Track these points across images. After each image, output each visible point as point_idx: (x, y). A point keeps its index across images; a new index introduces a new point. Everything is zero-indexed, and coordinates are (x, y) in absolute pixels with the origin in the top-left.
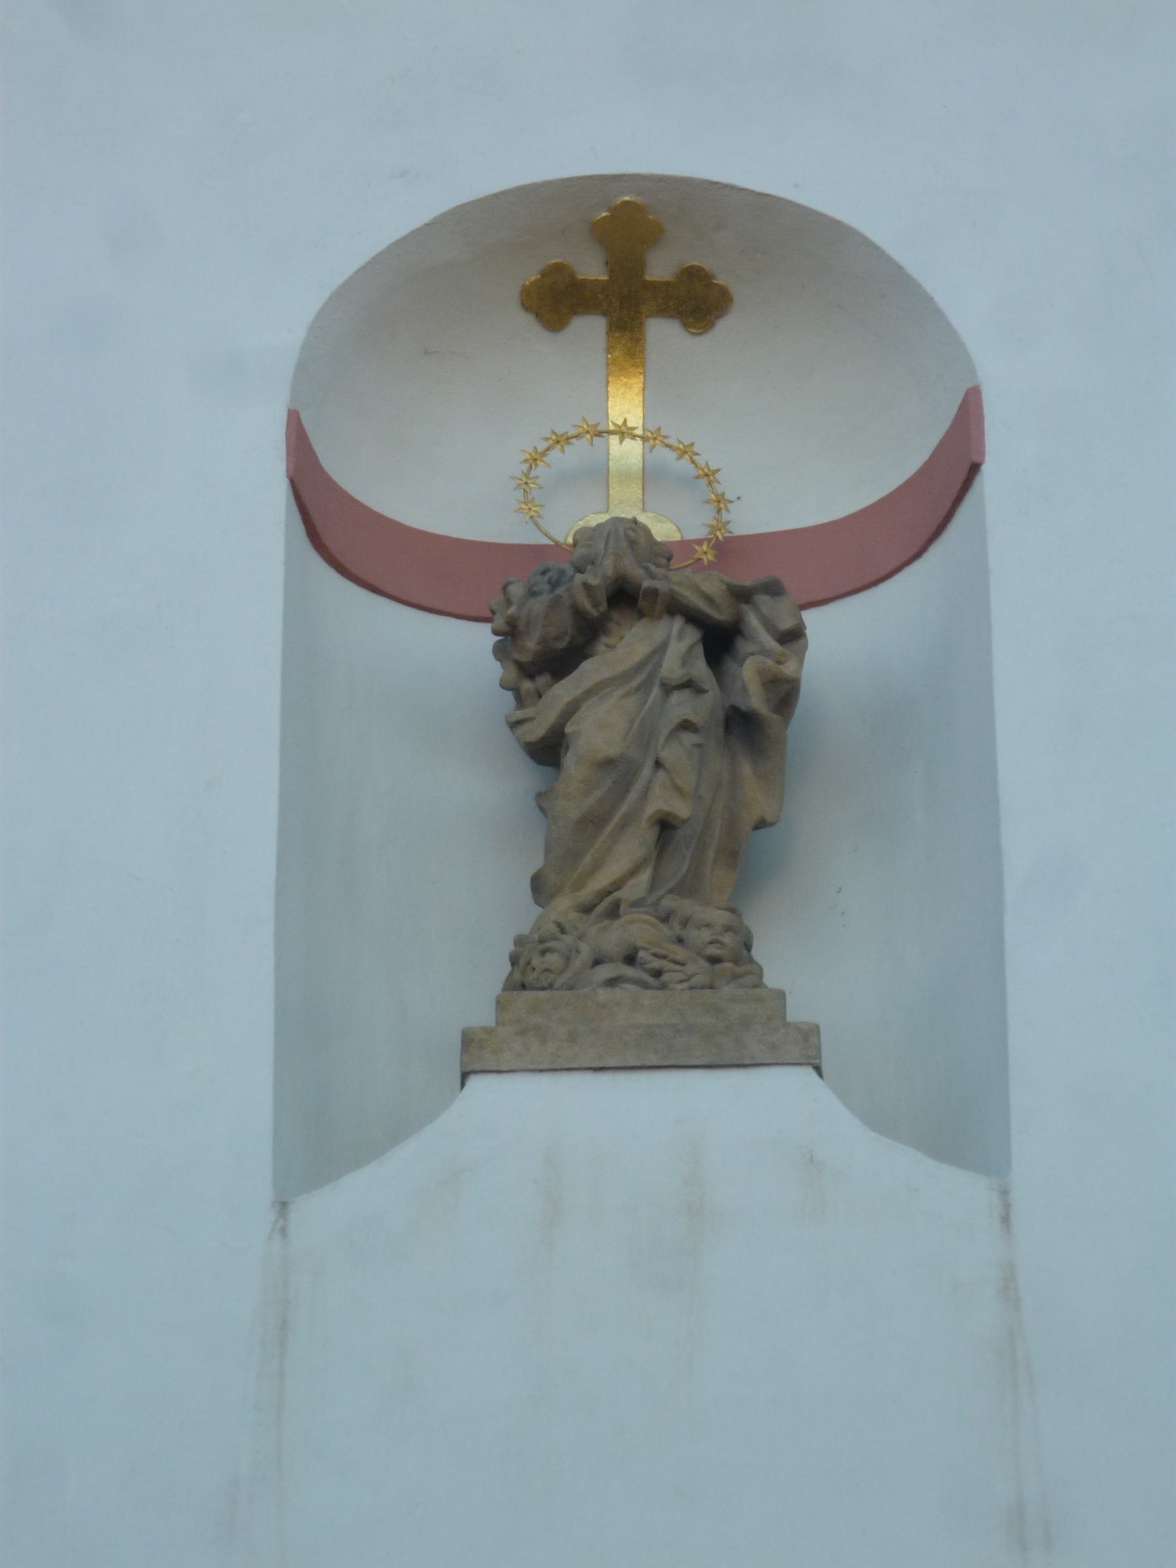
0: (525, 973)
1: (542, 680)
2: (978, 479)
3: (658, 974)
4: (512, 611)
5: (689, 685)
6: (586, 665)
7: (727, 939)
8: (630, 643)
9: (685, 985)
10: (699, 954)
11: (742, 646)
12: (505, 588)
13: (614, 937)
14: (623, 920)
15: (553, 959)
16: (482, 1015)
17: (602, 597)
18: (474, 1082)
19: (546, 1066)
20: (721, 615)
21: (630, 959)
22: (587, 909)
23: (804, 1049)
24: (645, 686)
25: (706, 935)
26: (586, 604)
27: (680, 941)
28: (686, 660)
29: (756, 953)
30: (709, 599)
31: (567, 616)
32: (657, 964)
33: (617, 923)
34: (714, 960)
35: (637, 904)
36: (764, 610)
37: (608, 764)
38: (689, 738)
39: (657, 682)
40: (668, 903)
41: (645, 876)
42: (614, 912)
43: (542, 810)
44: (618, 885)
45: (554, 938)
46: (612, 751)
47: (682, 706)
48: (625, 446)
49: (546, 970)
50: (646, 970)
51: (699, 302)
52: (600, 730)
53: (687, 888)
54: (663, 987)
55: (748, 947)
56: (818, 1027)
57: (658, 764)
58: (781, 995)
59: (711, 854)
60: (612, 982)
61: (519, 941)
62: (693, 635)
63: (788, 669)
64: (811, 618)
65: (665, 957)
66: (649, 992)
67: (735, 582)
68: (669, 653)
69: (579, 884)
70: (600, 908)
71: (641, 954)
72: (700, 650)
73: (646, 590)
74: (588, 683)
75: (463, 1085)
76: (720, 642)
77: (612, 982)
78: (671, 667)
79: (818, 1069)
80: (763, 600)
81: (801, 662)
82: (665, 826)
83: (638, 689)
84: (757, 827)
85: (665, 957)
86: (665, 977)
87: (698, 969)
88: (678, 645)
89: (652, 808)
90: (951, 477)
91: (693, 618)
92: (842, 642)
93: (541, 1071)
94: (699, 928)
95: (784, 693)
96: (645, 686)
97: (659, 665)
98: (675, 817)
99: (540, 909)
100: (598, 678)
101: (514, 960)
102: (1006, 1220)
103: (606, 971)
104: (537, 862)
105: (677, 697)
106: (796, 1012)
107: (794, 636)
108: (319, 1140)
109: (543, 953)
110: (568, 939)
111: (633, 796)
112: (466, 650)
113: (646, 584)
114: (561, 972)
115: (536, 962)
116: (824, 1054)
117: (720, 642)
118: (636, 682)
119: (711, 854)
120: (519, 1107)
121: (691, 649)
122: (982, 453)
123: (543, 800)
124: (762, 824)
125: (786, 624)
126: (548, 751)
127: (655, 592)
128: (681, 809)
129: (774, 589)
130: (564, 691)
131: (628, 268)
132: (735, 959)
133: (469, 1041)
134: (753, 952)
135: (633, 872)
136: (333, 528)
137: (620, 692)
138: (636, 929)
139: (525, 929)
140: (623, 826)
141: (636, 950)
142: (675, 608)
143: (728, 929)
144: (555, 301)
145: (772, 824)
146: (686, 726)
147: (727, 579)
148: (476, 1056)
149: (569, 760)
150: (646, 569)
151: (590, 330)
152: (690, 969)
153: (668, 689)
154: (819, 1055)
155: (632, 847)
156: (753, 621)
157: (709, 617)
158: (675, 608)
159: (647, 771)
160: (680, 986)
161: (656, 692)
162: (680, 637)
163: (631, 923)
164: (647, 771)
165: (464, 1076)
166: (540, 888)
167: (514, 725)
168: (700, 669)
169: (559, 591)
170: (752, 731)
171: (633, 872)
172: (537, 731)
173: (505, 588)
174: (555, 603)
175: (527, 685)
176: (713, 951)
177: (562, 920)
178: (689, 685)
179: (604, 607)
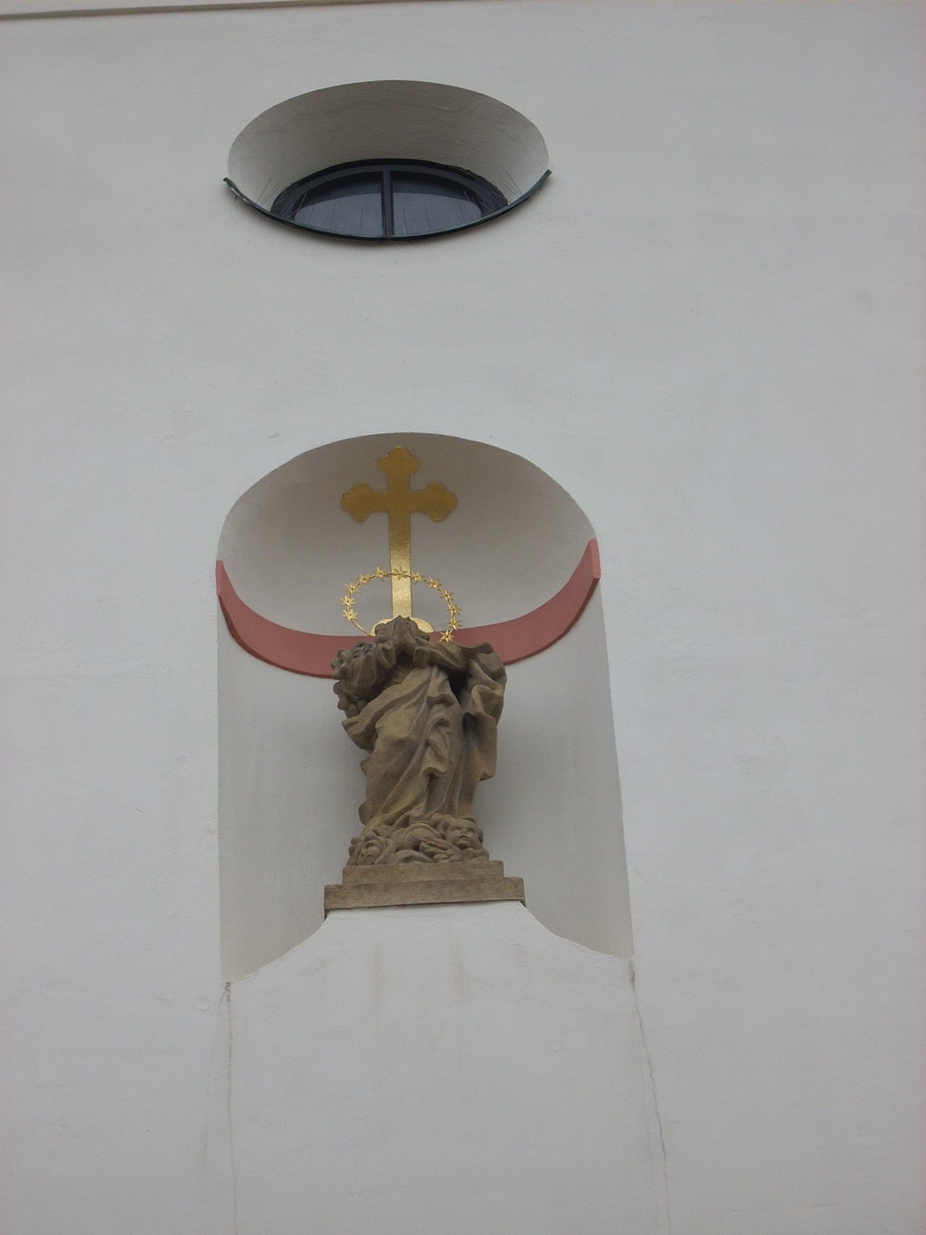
0: (358, 854)
1: (360, 704)
2: (597, 588)
3: (431, 855)
4: (343, 665)
5: (443, 701)
6: (387, 691)
7: (470, 835)
8: (411, 681)
9: (447, 860)
10: (454, 844)
11: (471, 682)
12: (339, 653)
13: (405, 835)
14: (411, 826)
15: (374, 849)
16: (336, 879)
17: (393, 656)
18: (331, 915)
19: (372, 905)
20: (458, 665)
21: (416, 848)
22: (390, 823)
23: (514, 891)
24: (419, 701)
25: (458, 833)
26: (384, 660)
27: (444, 837)
28: (441, 687)
29: (485, 845)
30: (451, 656)
31: (370, 673)
32: (432, 849)
33: (407, 829)
34: (463, 847)
35: (419, 818)
36: (483, 661)
37: (400, 743)
38: (444, 730)
39: (425, 699)
40: (436, 817)
41: (422, 805)
42: (406, 823)
43: (364, 770)
44: (409, 808)
45: (373, 838)
46: (402, 735)
47: (439, 713)
48: (401, 593)
49: (370, 855)
50: (425, 854)
51: (440, 504)
52: (396, 725)
53: (449, 809)
54: (436, 861)
55: (481, 840)
56: (522, 880)
57: (427, 744)
58: (500, 864)
59: (457, 795)
60: (407, 860)
61: (354, 841)
62: (442, 677)
63: (497, 692)
64: (509, 670)
65: (435, 846)
66: (428, 864)
67: (465, 646)
68: (431, 685)
69: (386, 810)
70: (398, 821)
71: (422, 844)
72: (448, 684)
73: (418, 651)
74: (387, 702)
75: (326, 917)
76: (459, 681)
77: (407, 860)
78: (433, 691)
79: (523, 902)
80: (482, 656)
81: (504, 688)
82: (432, 776)
83: (415, 704)
84: (482, 779)
85: (435, 846)
86: (436, 857)
87: (453, 851)
88: (436, 683)
89: (424, 767)
90: (579, 594)
91: (443, 668)
92: (528, 690)
93: (369, 908)
94: (453, 830)
95: (495, 707)
96: (418, 703)
97: (426, 691)
98: (438, 771)
99: (363, 826)
100: (393, 698)
101: (351, 851)
102: (633, 980)
103: (404, 853)
104: (363, 799)
105: (436, 708)
106: (509, 872)
107: (499, 677)
108: (254, 941)
109: (367, 847)
110: (382, 839)
111: (414, 760)
112: (319, 698)
113: (417, 648)
114: (379, 856)
115: (364, 851)
116: (526, 895)
117: (459, 681)
118: (414, 700)
119: (457, 795)
120: (343, 923)
121: (443, 682)
122: (599, 574)
123: (363, 765)
124: (485, 777)
125: (495, 668)
126: (367, 739)
127: (422, 652)
128: (441, 768)
129: (487, 649)
130: (375, 705)
131: (398, 485)
132: (471, 846)
133: (328, 892)
134: (483, 845)
135: (415, 803)
136: (241, 626)
137: (405, 705)
138: (420, 831)
139: (357, 835)
140: (410, 777)
141: (420, 842)
142: (433, 662)
143: (470, 830)
144: (359, 506)
145: (490, 777)
146: (442, 723)
147: (462, 645)
148: (335, 900)
149: (379, 744)
150: (417, 640)
151: (379, 522)
152: (449, 852)
153: (432, 703)
154: (523, 895)
155: (416, 788)
156: (476, 667)
157: (451, 665)
158: (433, 662)
159: (421, 747)
160: (444, 861)
161: (424, 705)
162: (437, 676)
163: (416, 828)
164: (421, 747)
165: (327, 912)
166: (365, 815)
167: (347, 727)
168: (449, 692)
169: (369, 654)
170: (477, 729)
171: (415, 803)
172: (361, 728)
173: (339, 653)
174: (368, 659)
175: (353, 707)
176: (462, 841)
177: (377, 829)
178: (443, 701)
179: (394, 661)
